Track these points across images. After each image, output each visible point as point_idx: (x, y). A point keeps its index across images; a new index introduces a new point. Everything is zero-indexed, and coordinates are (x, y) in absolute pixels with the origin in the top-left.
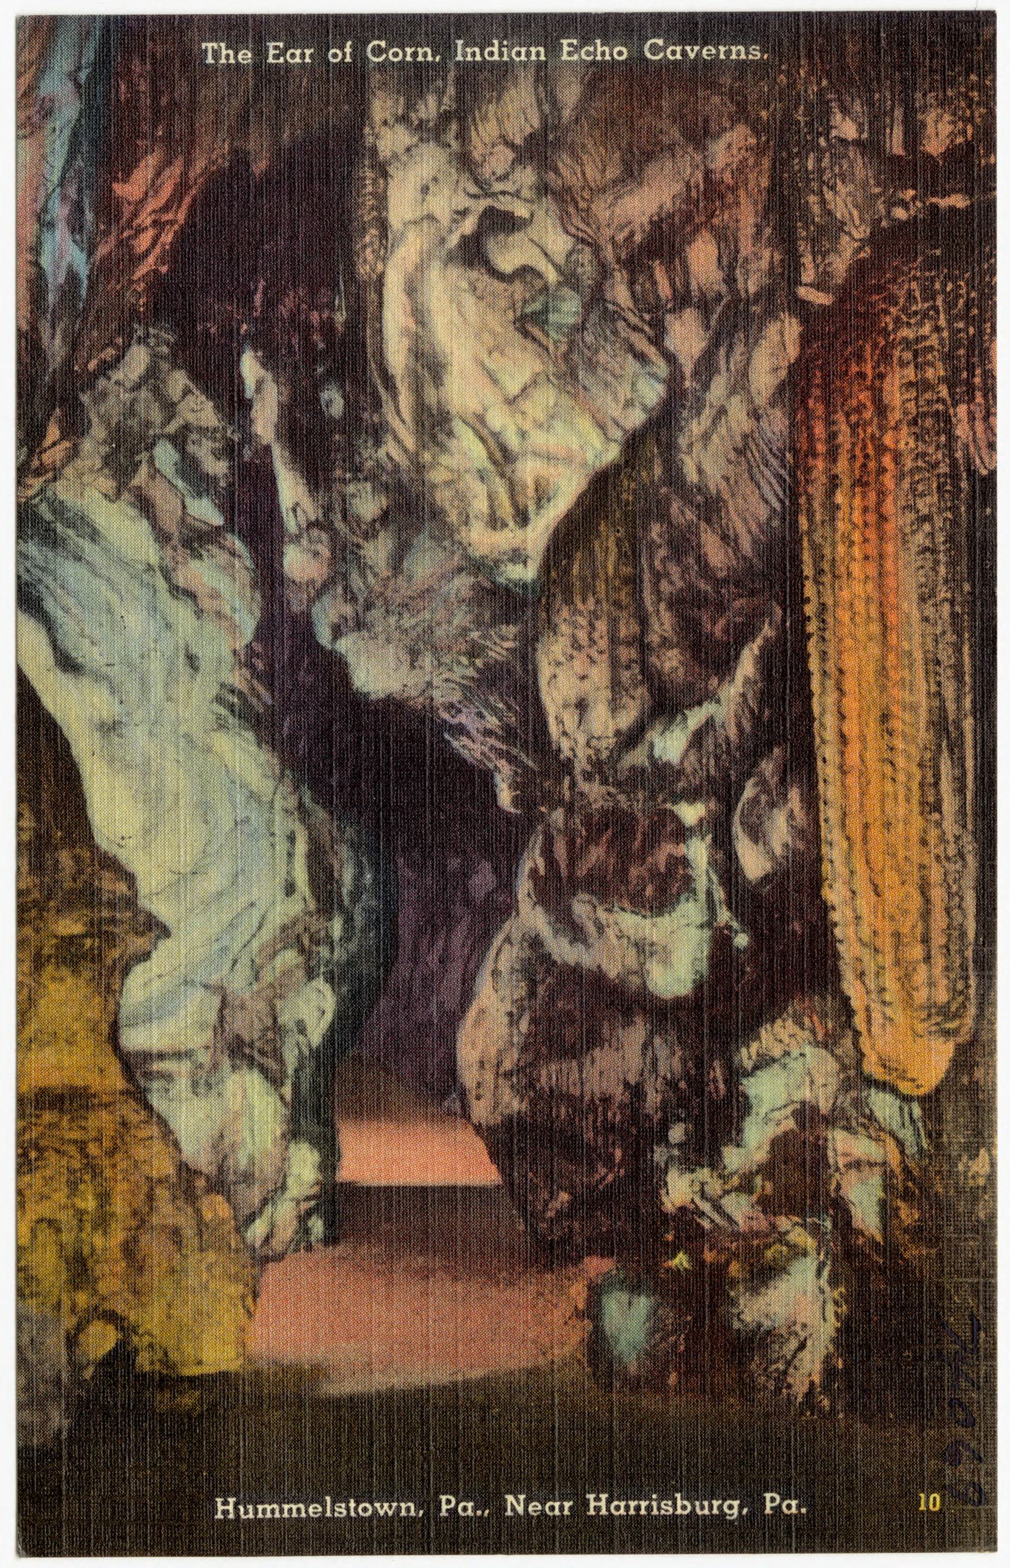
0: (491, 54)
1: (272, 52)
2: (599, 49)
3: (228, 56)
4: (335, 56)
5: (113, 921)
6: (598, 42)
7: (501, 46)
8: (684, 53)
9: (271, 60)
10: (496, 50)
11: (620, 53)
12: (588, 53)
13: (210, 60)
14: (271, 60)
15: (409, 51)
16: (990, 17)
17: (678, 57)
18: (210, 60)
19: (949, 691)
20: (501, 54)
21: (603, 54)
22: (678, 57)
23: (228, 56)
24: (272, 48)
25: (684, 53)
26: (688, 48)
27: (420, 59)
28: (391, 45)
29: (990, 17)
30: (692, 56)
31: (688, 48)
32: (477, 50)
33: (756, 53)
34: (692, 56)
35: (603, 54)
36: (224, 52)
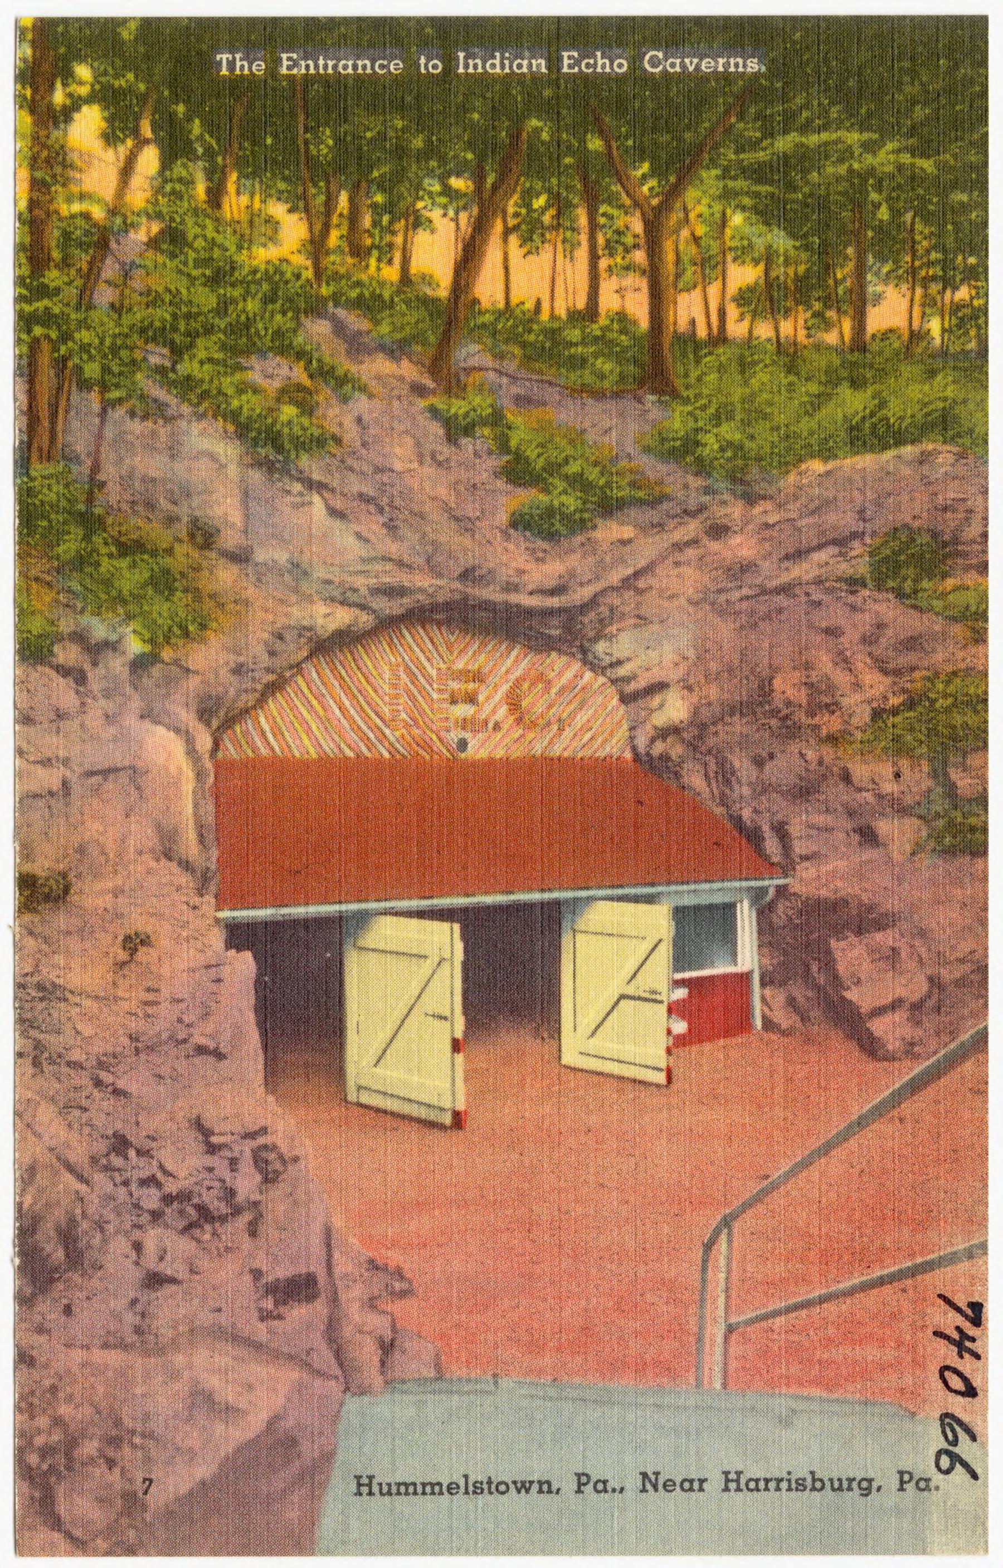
0: (493, 66)
1: (566, 62)
2: (600, 62)
3: (242, 67)
4: (435, 67)
5: (771, 404)
6: (599, 54)
7: (502, 58)
8: (683, 65)
9: (565, 70)
10: (497, 62)
11: (620, 66)
12: (588, 65)
13: (224, 72)
14: (565, 70)
15: (721, 61)
16: (975, 29)
17: (678, 69)
18: (224, 72)
19: (569, 272)
20: (503, 67)
21: (603, 66)
22: (678, 69)
23: (242, 67)
24: (567, 57)
25: (683, 65)
26: (687, 61)
27: (732, 69)
28: (583, 57)
29: (975, 29)
30: (691, 69)
31: (687, 61)
32: (368, 63)
33: (753, 66)
34: (691, 69)
35: (603, 66)
36: (238, 64)
